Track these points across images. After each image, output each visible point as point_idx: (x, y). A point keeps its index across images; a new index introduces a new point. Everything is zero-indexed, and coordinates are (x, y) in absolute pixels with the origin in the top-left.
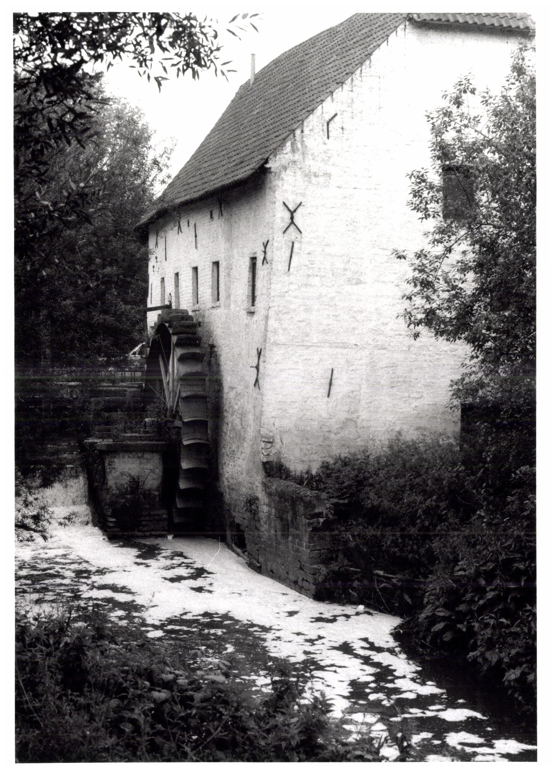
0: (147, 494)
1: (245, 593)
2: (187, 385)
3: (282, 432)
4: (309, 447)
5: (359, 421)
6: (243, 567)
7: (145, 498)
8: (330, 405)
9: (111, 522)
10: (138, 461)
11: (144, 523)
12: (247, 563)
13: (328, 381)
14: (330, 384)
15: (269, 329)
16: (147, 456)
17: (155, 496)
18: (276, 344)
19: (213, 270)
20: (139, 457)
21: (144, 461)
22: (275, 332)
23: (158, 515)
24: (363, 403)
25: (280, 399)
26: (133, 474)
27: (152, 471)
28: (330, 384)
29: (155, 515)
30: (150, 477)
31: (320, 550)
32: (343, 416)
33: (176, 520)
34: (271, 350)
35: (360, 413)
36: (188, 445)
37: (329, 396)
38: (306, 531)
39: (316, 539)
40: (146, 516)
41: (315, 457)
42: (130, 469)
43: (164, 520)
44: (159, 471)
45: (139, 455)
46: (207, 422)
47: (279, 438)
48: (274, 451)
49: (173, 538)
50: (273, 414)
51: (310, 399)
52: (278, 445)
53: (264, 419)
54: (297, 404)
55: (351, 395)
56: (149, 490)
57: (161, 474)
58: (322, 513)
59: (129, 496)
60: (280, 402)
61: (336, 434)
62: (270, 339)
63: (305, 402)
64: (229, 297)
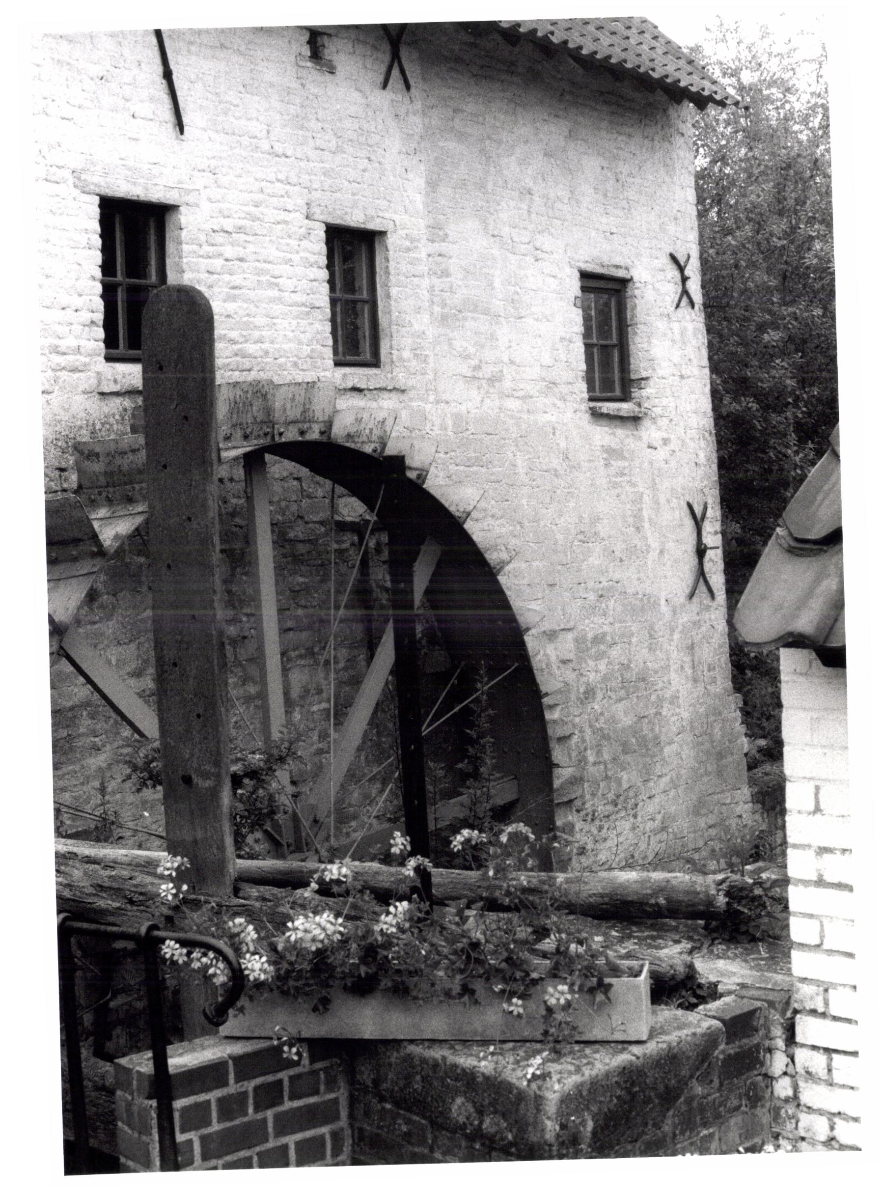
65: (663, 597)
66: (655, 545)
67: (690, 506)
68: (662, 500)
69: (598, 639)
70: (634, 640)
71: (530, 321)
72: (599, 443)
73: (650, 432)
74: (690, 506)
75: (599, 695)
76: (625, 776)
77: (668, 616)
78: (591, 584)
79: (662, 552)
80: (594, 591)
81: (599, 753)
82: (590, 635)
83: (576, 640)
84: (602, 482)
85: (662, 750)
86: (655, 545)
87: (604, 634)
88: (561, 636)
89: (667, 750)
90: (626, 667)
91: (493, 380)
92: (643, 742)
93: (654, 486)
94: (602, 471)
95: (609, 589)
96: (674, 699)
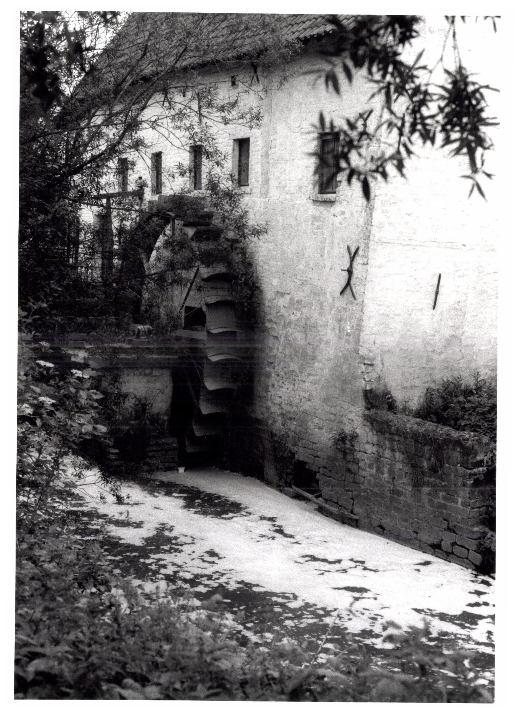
0: (155, 419)
1: (305, 541)
2: (212, 288)
3: (383, 353)
4: (411, 370)
5: (463, 338)
6: (316, 514)
7: (152, 424)
8: (435, 319)
9: (113, 454)
10: (145, 379)
11: (151, 454)
12: (316, 510)
13: (435, 289)
14: (437, 293)
15: (375, 221)
16: (155, 372)
17: (164, 421)
18: (381, 242)
19: (234, 150)
20: (146, 375)
21: (153, 379)
22: (380, 227)
23: (167, 444)
24: (468, 316)
25: (382, 311)
26: (138, 396)
27: (162, 392)
28: (437, 293)
29: (164, 444)
30: (159, 399)
31: (479, 508)
32: (447, 332)
33: (190, 450)
34: (375, 250)
35: (466, 329)
36: (217, 363)
37: (434, 307)
38: (464, 485)
39: (476, 494)
40: (153, 445)
41: (417, 382)
42: (135, 389)
43: (174, 449)
44: (168, 391)
45: (148, 371)
46: (236, 332)
47: (379, 359)
48: (374, 375)
49: (185, 471)
50: (375, 330)
51: (414, 312)
52: (378, 369)
53: (365, 336)
54: (401, 318)
55: (456, 306)
56: (158, 414)
57: (170, 395)
58: (482, 461)
59: (133, 422)
60: (383, 314)
61: (440, 353)
62: (374, 236)
63: (410, 315)
64: (266, 181)
65: (329, 290)
66: (328, 265)
67: (348, 249)
68: (336, 243)
69: (299, 302)
70: (313, 307)
71: (297, 160)
72: (311, 213)
73: (337, 209)
74: (348, 249)
75: (293, 326)
76: (292, 364)
77: (330, 301)
78: (299, 277)
79: (331, 269)
80: (300, 280)
81: (284, 349)
82: (296, 299)
83: (290, 299)
84: (309, 231)
85: (314, 363)
86: (328, 265)
87: (301, 301)
88: (286, 296)
89: (317, 364)
90: (308, 319)
91: (284, 187)
92: (305, 355)
93: (332, 235)
94: (310, 226)
95: (306, 281)
96: (328, 343)
